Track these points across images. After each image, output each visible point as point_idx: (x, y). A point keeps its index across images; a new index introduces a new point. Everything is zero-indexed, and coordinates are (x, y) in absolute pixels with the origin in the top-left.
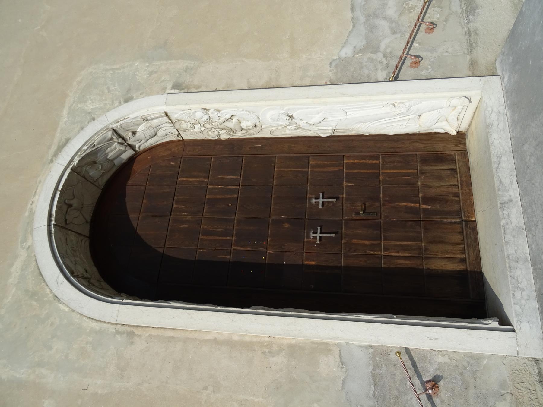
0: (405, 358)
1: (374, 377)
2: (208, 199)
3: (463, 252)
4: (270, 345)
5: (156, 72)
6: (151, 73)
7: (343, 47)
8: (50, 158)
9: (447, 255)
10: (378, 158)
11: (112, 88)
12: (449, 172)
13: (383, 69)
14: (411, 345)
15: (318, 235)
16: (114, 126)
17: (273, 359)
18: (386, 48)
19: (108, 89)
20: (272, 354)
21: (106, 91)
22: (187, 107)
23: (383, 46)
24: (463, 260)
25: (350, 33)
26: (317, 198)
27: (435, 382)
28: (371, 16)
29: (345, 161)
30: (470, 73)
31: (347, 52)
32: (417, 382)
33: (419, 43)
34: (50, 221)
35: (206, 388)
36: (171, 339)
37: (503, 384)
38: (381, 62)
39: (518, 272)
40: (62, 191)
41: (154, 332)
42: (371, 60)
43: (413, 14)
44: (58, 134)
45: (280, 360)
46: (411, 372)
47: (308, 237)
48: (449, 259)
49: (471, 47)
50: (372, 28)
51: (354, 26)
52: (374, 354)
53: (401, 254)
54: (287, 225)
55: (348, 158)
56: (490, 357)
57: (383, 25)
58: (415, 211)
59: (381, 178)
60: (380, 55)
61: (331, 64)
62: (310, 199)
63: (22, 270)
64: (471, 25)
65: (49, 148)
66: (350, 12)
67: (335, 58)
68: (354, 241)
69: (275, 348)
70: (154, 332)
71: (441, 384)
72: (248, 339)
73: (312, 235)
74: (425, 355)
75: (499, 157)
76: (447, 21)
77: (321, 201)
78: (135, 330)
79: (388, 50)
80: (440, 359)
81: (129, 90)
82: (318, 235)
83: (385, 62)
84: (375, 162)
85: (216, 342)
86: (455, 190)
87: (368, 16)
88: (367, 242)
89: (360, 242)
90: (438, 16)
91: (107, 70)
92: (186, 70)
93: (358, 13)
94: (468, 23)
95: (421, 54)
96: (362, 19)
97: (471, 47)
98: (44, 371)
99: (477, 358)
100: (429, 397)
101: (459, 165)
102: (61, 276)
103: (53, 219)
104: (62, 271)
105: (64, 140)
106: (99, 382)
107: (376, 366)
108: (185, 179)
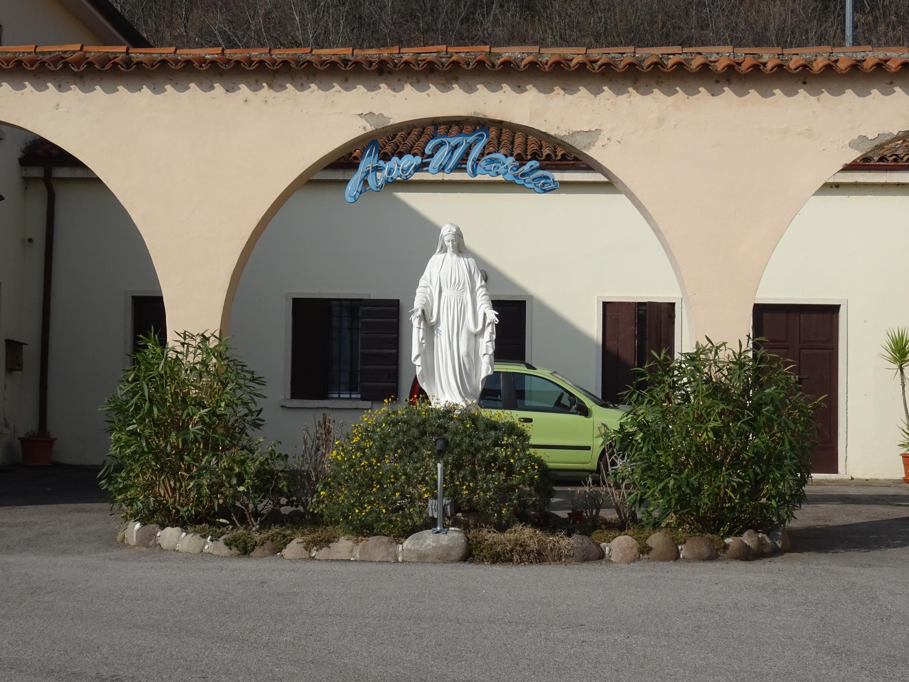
30: (526, 376)
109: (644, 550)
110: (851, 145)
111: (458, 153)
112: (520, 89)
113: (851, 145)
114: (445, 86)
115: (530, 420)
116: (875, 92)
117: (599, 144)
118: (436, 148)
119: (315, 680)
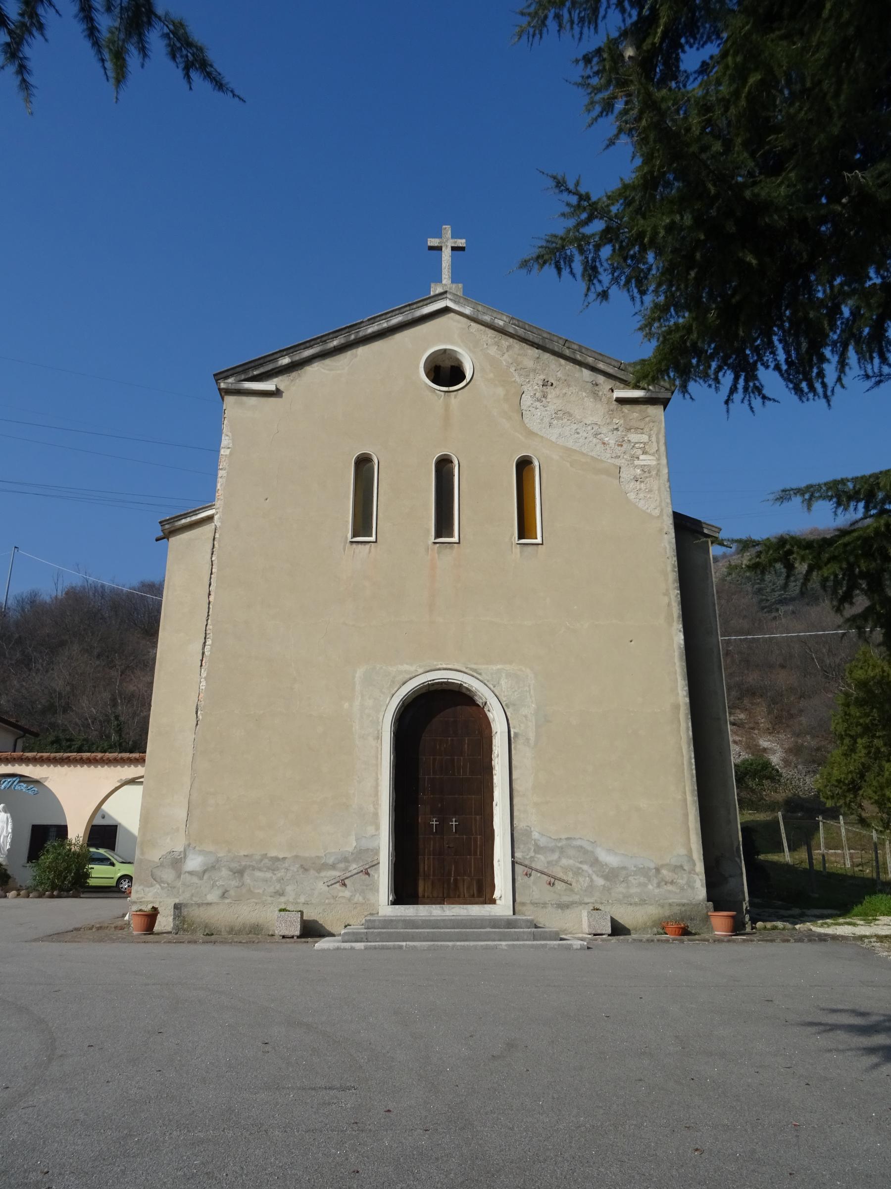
0: (376, 863)
1: (368, 849)
2: (454, 759)
3: (428, 897)
4: (378, 804)
5: (526, 720)
6: (526, 716)
7: (539, 833)
8: (469, 666)
9: (426, 889)
10: (481, 854)
11: (516, 693)
12: (472, 893)
13: (523, 856)
14: (381, 865)
15: (454, 823)
16: (488, 703)
17: (371, 806)
18: (537, 858)
19: (516, 691)
20: (374, 805)
21: (513, 690)
22: (499, 746)
23: (539, 856)
24: (424, 896)
25: (550, 838)
26: (455, 822)
27: (368, 874)
28: (562, 850)
29: (479, 837)
31: (535, 835)
32: (367, 867)
33: (539, 877)
34: (430, 681)
35: (358, 777)
36: (377, 758)
37: (368, 900)
38: (528, 855)
39: (412, 910)
40: (448, 682)
41: (379, 749)
42: (529, 850)
43: (562, 874)
44: (484, 667)
45: (372, 809)
46: (371, 864)
47: (434, 817)
48: (424, 890)
49: (532, 904)
50: (552, 850)
51: (554, 839)
52: (377, 849)
53: (426, 866)
54: (439, 805)
55: (481, 838)
56: (378, 896)
57: (555, 857)
58: (449, 874)
59: (468, 857)
60: (532, 854)
61: (528, 826)
62: (455, 818)
63: (405, 671)
64: (550, 905)
65: (475, 664)
66: (566, 837)
67: (532, 829)
68: (432, 842)
69: (376, 806)
70: (379, 749)
71: (367, 876)
72: (379, 794)
73: (434, 820)
74: (378, 870)
75: (466, 909)
76: (555, 892)
77: (454, 823)
78: (380, 739)
79: (536, 859)
80: (376, 876)
81: (514, 705)
82: (434, 823)
83: (528, 857)
84: (478, 853)
85: (377, 779)
86: (462, 896)
87: (562, 848)
88: (431, 849)
89: (432, 846)
90: (559, 888)
91: (529, 686)
92: (528, 740)
93: (564, 842)
94: (551, 904)
95: (532, 878)
96: (560, 845)
97: (532, 904)
98: (360, 698)
99: (378, 891)
100: (362, 871)
101: (477, 899)
102: (402, 697)
103: (432, 682)
104: (406, 695)
105: (480, 672)
106: (357, 727)
107: (372, 850)
108: (466, 742)
109: (18, 895)
110: (118, 781)
111: (10, 783)
112: (27, 765)
113: (118, 781)
114: (6, 765)
115: (93, 868)
116: (119, 766)
117: (47, 781)
118: (4, 782)
119: (642, 1188)
